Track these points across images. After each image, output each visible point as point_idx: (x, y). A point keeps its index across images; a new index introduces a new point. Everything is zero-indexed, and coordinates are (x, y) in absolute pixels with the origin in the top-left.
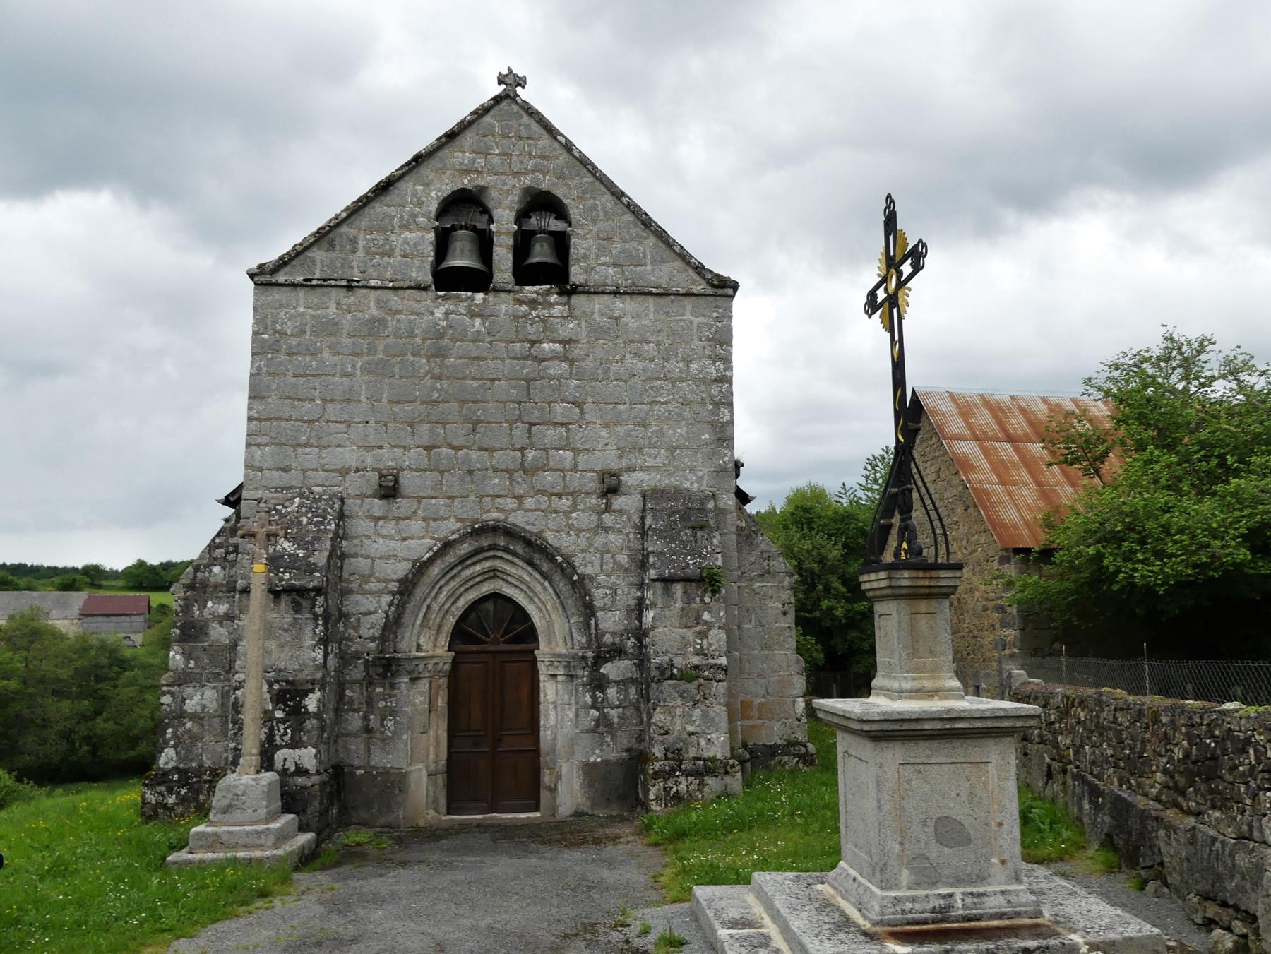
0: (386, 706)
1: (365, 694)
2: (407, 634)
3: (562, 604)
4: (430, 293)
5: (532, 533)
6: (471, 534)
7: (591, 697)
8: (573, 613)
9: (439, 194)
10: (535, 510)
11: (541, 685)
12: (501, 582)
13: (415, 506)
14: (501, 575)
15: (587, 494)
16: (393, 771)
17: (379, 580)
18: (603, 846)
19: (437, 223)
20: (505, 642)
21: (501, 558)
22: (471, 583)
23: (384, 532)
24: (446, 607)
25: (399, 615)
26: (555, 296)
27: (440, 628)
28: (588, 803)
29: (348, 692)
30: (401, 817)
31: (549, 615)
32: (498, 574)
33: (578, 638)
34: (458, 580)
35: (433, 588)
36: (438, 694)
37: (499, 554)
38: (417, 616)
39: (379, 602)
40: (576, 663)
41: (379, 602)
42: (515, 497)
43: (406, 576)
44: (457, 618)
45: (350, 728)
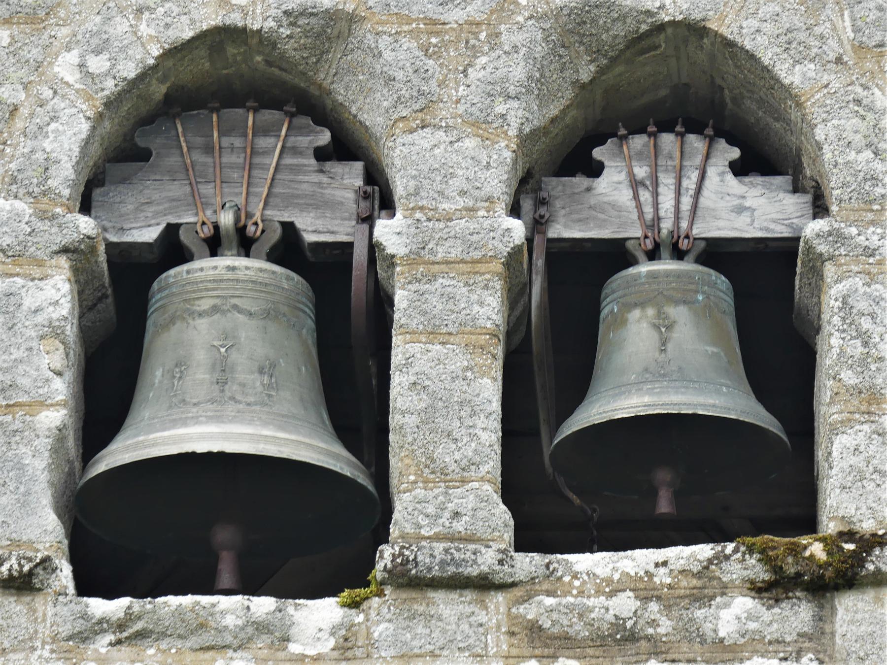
4: (43, 605)
9: (97, 64)
19: (86, 224)
26: (744, 604)
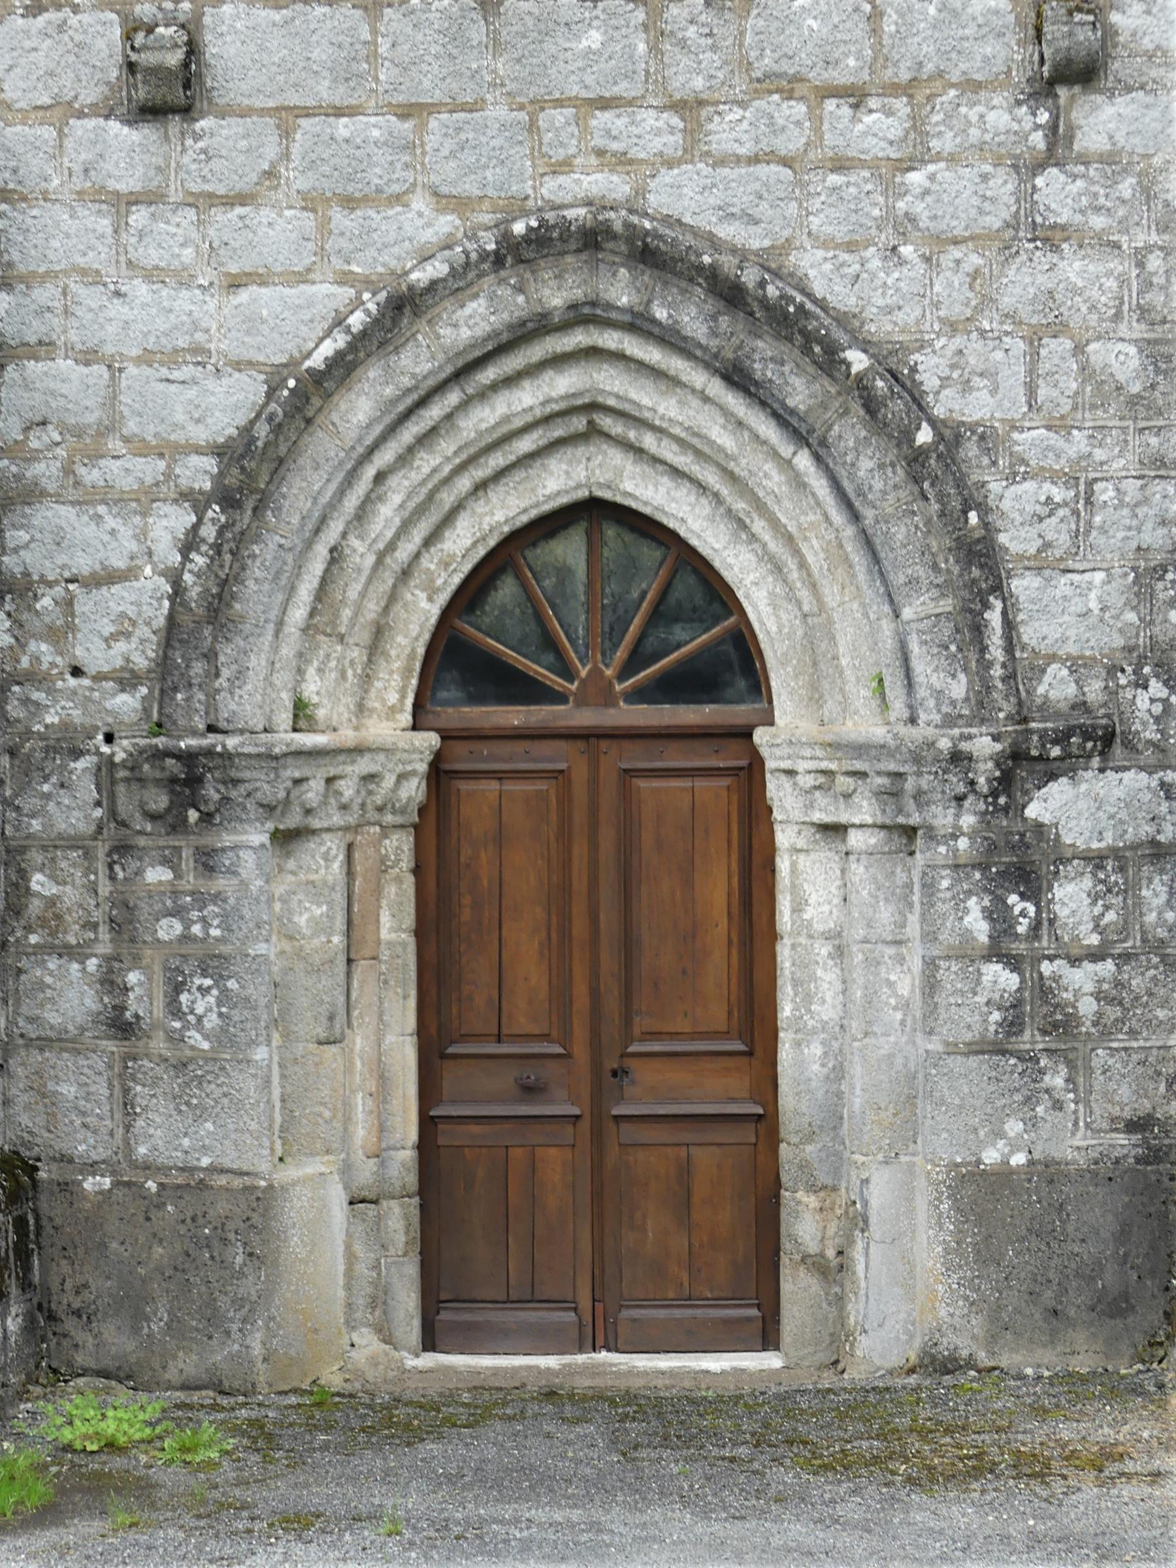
0: (186, 938)
1: (105, 889)
2: (257, 662)
3: (867, 542)
5: (742, 255)
6: (498, 260)
7: (988, 914)
8: (912, 582)
10: (754, 160)
11: (783, 864)
12: (616, 457)
13: (271, 151)
14: (616, 428)
15: (971, 87)
16: (222, 1180)
17: (141, 448)
18: (1058, 1486)
20: (639, 695)
21: (619, 357)
22: (497, 460)
23: (151, 255)
24: (404, 552)
25: (224, 583)
27: (380, 633)
28: (977, 1323)
29: (38, 882)
30: (257, 1350)
31: (814, 587)
32: (606, 422)
33: (937, 680)
34: (447, 446)
35: (351, 477)
36: (378, 892)
37: (610, 339)
38: (292, 590)
39: (142, 535)
40: (925, 782)
41: (142, 535)
42: (678, 106)
43: (247, 430)
44: (443, 598)
45: (52, 1017)
